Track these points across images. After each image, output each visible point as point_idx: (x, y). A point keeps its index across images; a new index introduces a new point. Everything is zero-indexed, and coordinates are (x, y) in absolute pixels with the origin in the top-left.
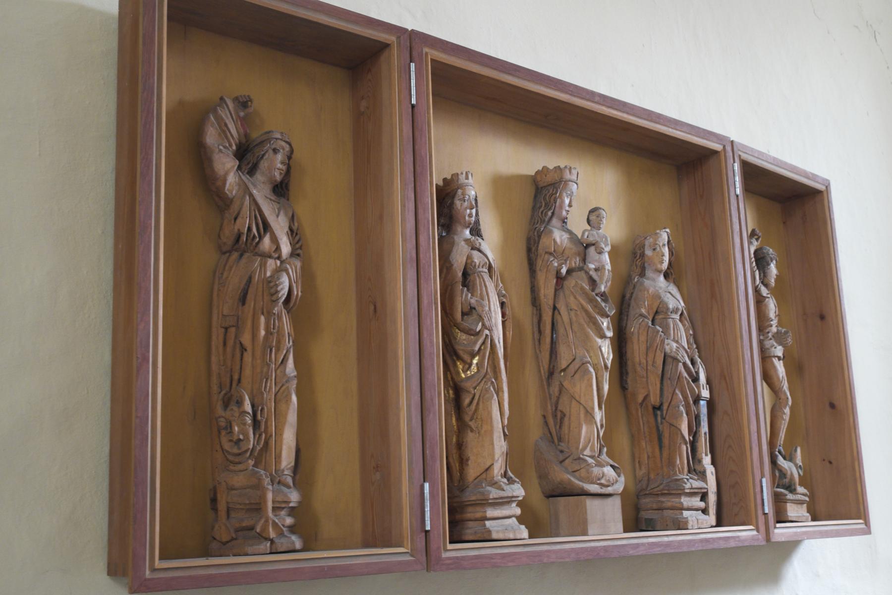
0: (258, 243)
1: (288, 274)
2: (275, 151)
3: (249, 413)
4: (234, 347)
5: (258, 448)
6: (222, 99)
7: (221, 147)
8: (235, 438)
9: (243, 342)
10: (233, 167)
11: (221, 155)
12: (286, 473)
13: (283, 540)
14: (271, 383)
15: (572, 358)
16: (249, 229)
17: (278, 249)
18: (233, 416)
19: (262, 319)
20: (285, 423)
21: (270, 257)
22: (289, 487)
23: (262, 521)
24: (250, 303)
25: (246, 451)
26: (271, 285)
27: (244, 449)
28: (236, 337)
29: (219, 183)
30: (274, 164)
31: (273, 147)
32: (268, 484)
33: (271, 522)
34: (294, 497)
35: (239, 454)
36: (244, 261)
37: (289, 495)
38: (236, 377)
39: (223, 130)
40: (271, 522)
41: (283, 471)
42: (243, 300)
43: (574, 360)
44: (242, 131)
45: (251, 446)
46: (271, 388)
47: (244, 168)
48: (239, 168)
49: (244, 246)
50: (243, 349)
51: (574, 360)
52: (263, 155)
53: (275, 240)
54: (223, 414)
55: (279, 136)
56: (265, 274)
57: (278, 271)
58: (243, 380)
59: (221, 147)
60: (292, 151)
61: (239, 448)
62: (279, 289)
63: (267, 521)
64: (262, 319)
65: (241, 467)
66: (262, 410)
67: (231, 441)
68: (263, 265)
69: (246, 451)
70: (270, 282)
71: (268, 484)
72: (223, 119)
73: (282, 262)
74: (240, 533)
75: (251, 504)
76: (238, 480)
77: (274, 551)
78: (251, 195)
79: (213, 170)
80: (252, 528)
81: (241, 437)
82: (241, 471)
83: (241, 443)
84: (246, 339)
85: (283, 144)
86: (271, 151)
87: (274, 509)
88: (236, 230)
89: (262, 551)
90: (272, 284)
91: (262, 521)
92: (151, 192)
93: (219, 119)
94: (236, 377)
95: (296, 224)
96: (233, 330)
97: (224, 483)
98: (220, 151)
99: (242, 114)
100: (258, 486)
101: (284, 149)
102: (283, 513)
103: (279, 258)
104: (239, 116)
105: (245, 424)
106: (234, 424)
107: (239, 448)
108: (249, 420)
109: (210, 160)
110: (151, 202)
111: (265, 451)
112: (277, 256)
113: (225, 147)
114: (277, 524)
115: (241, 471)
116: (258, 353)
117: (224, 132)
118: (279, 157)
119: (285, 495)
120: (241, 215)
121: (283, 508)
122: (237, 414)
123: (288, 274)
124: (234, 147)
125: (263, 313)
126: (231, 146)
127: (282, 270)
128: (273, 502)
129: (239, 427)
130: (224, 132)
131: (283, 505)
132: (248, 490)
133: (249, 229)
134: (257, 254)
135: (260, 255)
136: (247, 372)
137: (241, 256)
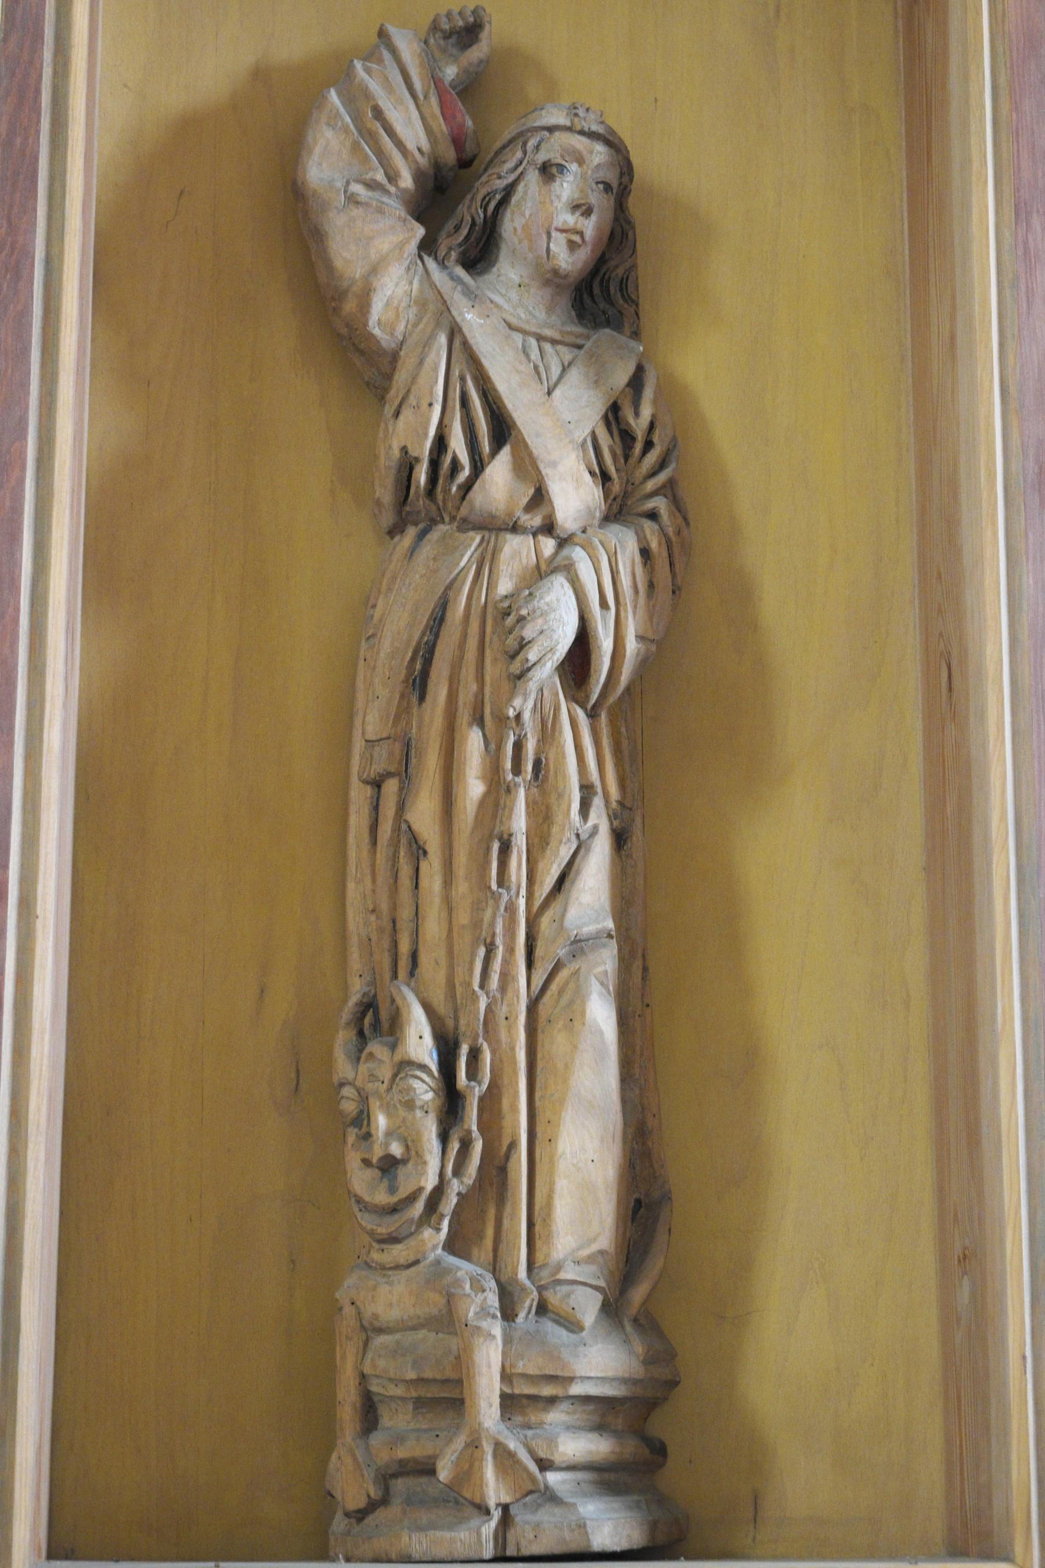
0: (467, 487)
1: (575, 583)
2: (548, 171)
3: (423, 1067)
4: (395, 843)
5: (455, 1187)
6: (382, 34)
7: (357, 188)
8: (377, 1153)
9: (415, 827)
10: (401, 246)
11: (356, 212)
12: (569, 1273)
13: (547, 1516)
14: (507, 962)
15: (412, 1258)
16: (441, 443)
17: (540, 497)
18: (372, 1077)
19: (474, 742)
20: (562, 1101)
21: (515, 528)
22: (573, 1326)
23: (460, 1442)
24: (439, 691)
25: (412, 1198)
26: (507, 621)
27: (403, 1193)
28: (401, 807)
29: (350, 306)
30: (552, 218)
31: (542, 157)
32: (484, 1312)
33: (488, 1449)
34: (600, 1362)
35: (394, 1210)
36: (427, 550)
37: (565, 1354)
38: (404, 947)
39: (371, 125)
40: (488, 1449)
41: (559, 1267)
42: (418, 683)
43: (416, 1262)
44: (441, 126)
45: (430, 1182)
46: (506, 977)
47: (443, 246)
48: (427, 246)
49: (425, 498)
50: (418, 851)
51: (416, 1262)
52: (509, 191)
53: (527, 467)
54: (350, 1076)
55: (559, 118)
56: (491, 586)
57: (540, 573)
58: (424, 959)
59: (357, 188)
60: (625, 168)
61: (392, 1190)
62: (528, 633)
63: (474, 1444)
64: (474, 742)
65: (399, 1253)
66: (474, 1055)
67: (367, 1163)
68: (487, 560)
69: (412, 1198)
70: (507, 613)
71: (484, 1312)
72: (367, 95)
73: (563, 542)
74: (400, 1485)
75: (420, 1381)
76: (392, 1299)
77: (510, 1552)
78: (455, 332)
79: (330, 267)
80: (429, 1470)
81: (396, 1149)
82: (397, 1267)
83: (402, 1172)
84: (424, 815)
85: (580, 143)
86: (533, 177)
87: (510, 1403)
88: (396, 453)
89: (460, 1552)
90: (510, 621)
91: (460, 1442)
92: (26, 351)
93: (357, 99)
94: (404, 947)
95: (647, 412)
96: (391, 786)
97: (348, 1310)
98: (352, 200)
99: (450, 72)
100: (447, 1320)
101: (580, 161)
102: (556, 1416)
103: (549, 528)
104: (437, 82)
105: (410, 1105)
106: (374, 1104)
107: (392, 1190)
108: (425, 1090)
109: (318, 235)
110: (25, 385)
111: (490, 1197)
112: (537, 521)
113: (372, 185)
114: (512, 1455)
115: (397, 1267)
116: (461, 859)
117: (371, 137)
118: (566, 188)
119: (554, 1356)
120: (412, 400)
121: (552, 1401)
122: (386, 1073)
123: (575, 583)
124: (407, 181)
125: (480, 722)
126: (392, 177)
127: (554, 571)
128: (506, 1377)
129: (389, 1115)
130: (371, 137)
131: (547, 1391)
132: (422, 1333)
133: (441, 443)
134: (467, 525)
135: (479, 527)
136: (433, 927)
137: (422, 535)
